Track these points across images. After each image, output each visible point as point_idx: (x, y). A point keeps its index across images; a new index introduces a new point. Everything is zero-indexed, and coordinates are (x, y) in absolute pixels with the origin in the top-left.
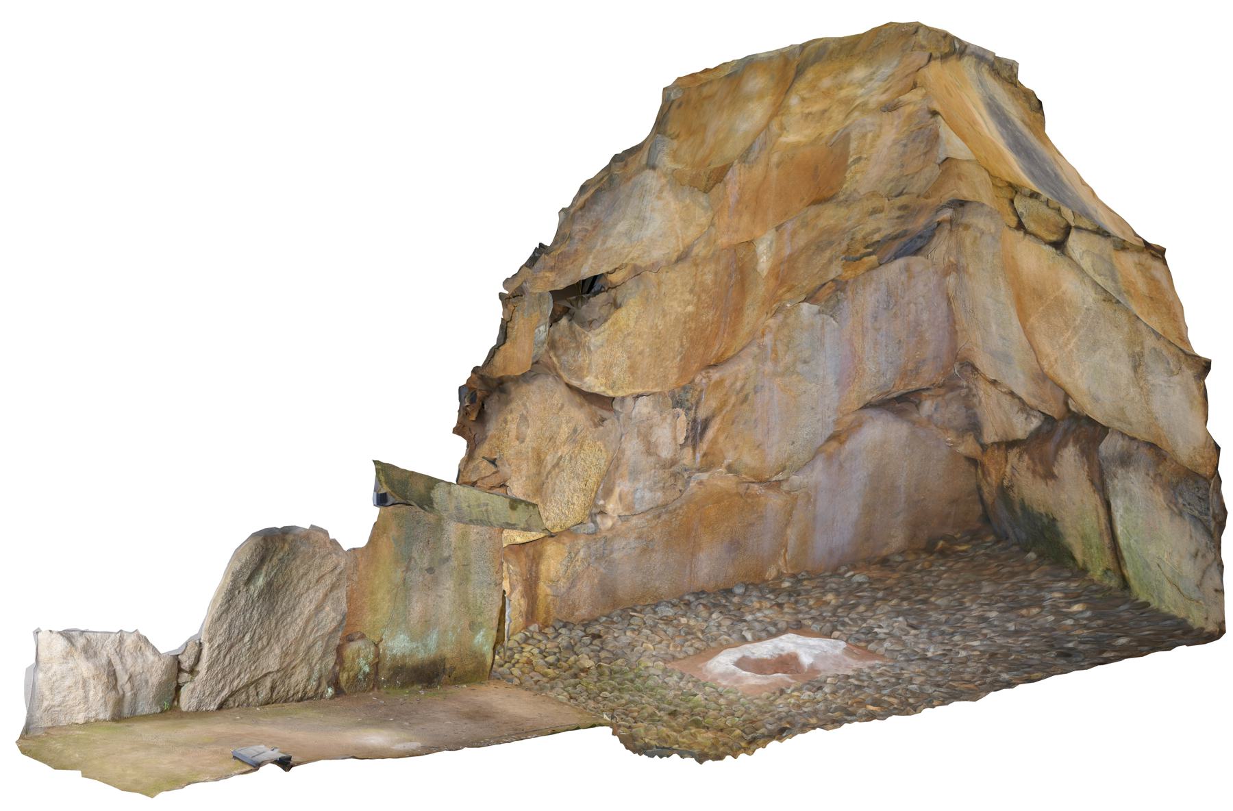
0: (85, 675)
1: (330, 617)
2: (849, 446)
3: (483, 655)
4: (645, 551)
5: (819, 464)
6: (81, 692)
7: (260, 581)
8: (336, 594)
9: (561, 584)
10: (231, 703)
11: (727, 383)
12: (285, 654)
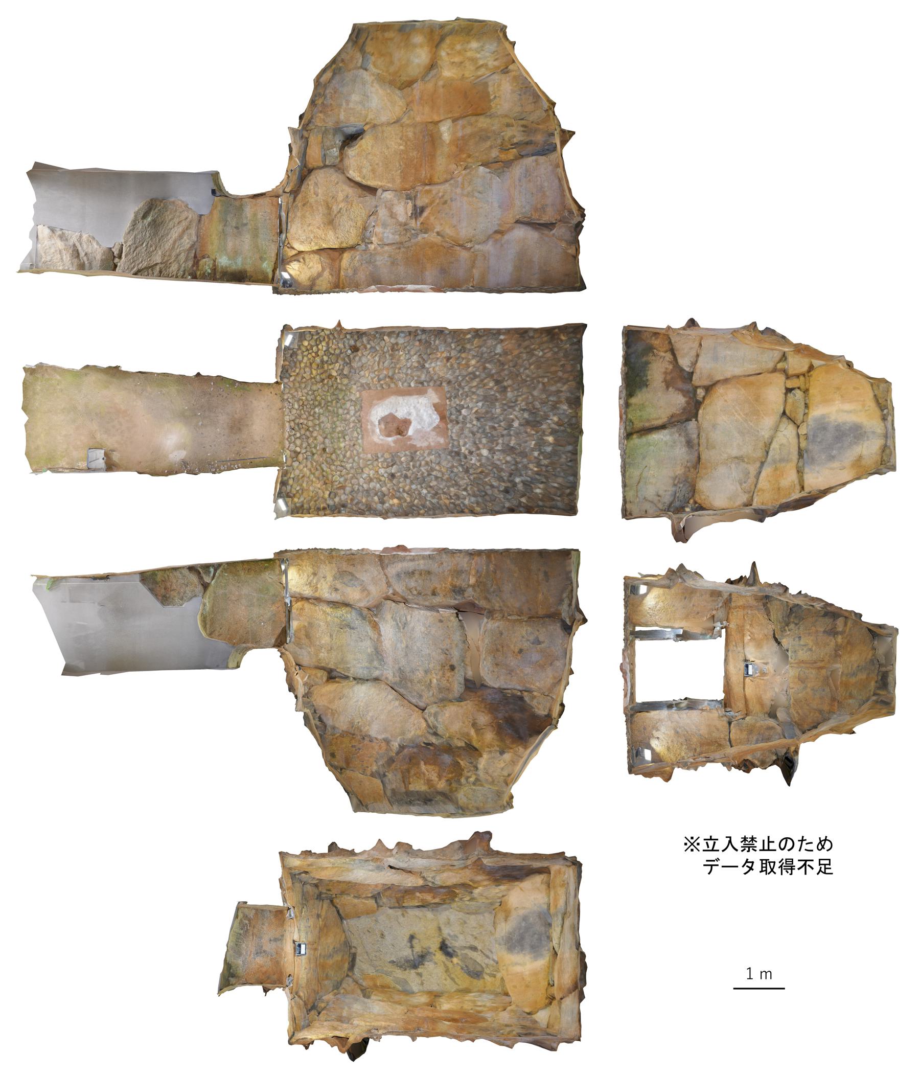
1: (186, 242)
2: (506, 237)
4: (393, 263)
5: (490, 243)
7: (149, 219)
8: (189, 231)
12: (164, 255)
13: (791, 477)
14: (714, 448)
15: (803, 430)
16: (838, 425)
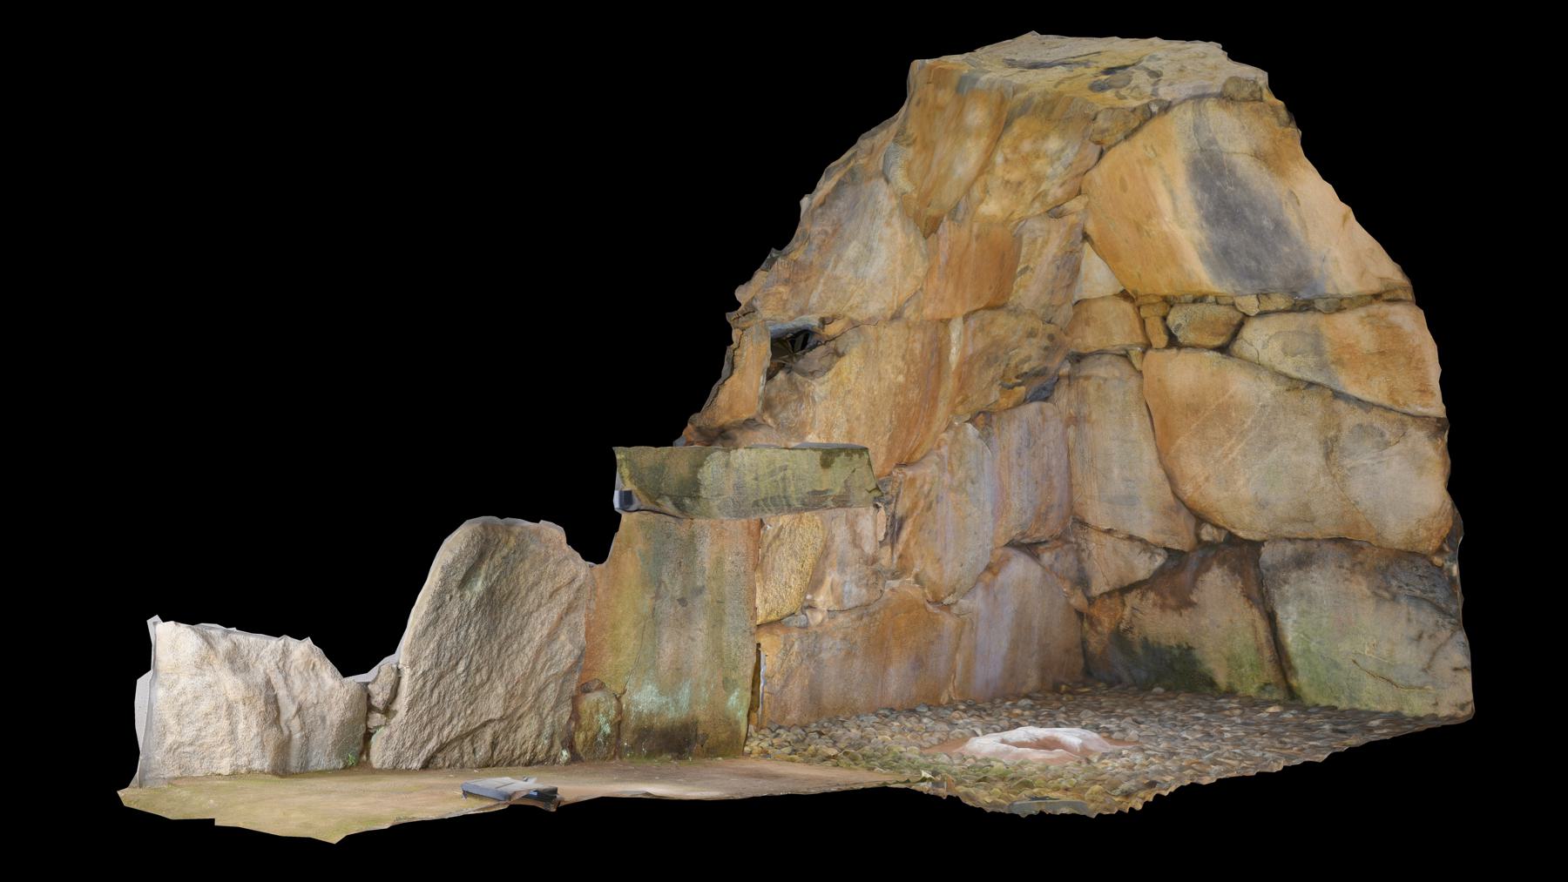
0: (231, 697)
1: (566, 650)
2: (1001, 578)
3: (737, 723)
6: (225, 723)
7: (479, 586)
9: (775, 680)
10: (439, 761)
11: (918, 483)
12: (510, 695)
13: (1350, 325)
14: (1306, 505)
15: (1250, 304)
16: (1206, 218)
